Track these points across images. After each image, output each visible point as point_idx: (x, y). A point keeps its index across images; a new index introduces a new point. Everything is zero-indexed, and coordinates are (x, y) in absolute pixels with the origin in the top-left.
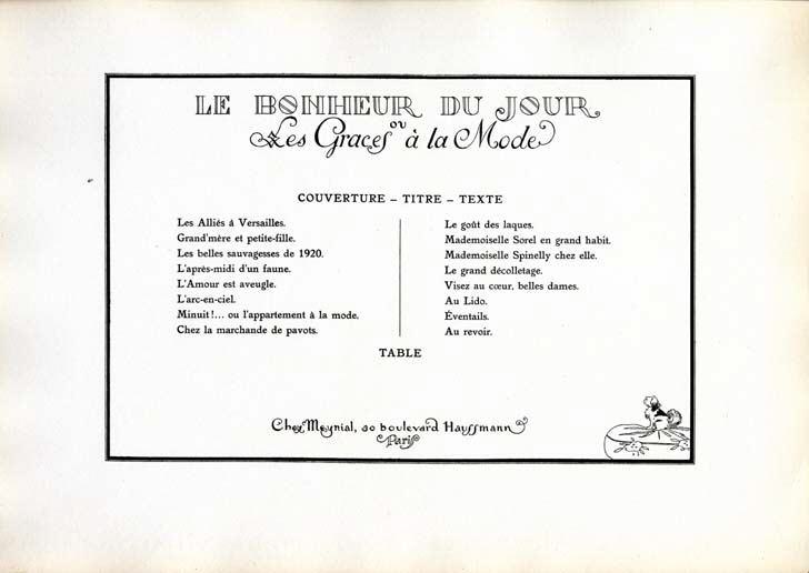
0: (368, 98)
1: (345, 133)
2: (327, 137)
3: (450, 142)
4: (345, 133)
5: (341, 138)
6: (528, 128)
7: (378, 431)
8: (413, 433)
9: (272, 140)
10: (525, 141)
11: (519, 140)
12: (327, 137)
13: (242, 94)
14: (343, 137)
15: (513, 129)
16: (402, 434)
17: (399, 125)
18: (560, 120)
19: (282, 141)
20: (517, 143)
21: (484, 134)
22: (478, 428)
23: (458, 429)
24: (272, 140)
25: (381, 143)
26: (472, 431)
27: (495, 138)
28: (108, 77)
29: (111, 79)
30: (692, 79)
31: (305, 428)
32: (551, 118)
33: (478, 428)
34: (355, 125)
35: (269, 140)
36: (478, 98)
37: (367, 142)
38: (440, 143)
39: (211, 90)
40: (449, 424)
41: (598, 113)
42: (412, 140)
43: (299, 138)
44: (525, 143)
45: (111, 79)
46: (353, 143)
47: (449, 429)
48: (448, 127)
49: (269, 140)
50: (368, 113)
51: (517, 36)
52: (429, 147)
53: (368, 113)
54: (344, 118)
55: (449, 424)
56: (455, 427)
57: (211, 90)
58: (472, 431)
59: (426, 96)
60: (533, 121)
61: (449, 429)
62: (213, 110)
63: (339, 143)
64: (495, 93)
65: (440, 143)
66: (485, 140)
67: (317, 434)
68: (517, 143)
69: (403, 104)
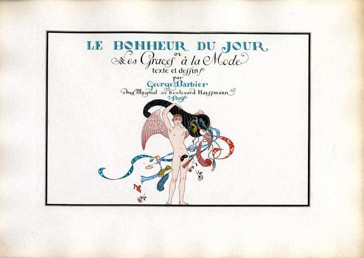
0: (164, 42)
2: (146, 60)
3: (201, 62)
7: (170, 69)
8: (184, 95)
9: (122, 61)
10: (235, 62)
11: (232, 61)
12: (146, 60)
15: (229, 56)
16: (179, 96)
17: (178, 54)
18: (250, 51)
19: (126, 62)
20: (231, 63)
23: (204, 93)
24: (122, 61)
25: (170, 62)
26: (210, 95)
27: (221, 60)
31: (135, 93)
32: (246, 51)
33: (213, 93)
35: (120, 61)
36: (214, 43)
37: (164, 62)
39: (93, 37)
40: (200, 91)
42: (184, 61)
43: (133, 60)
44: (235, 62)
46: (158, 62)
47: (200, 93)
49: (120, 61)
50: (165, 49)
51: (231, 14)
52: (192, 64)
53: (165, 49)
54: (154, 51)
55: (200, 91)
57: (93, 37)
58: (210, 95)
59: (191, 42)
60: (238, 53)
61: (200, 93)
62: (95, 48)
63: (151, 62)
64: (222, 40)
67: (141, 95)
68: (231, 63)
69: (180, 45)
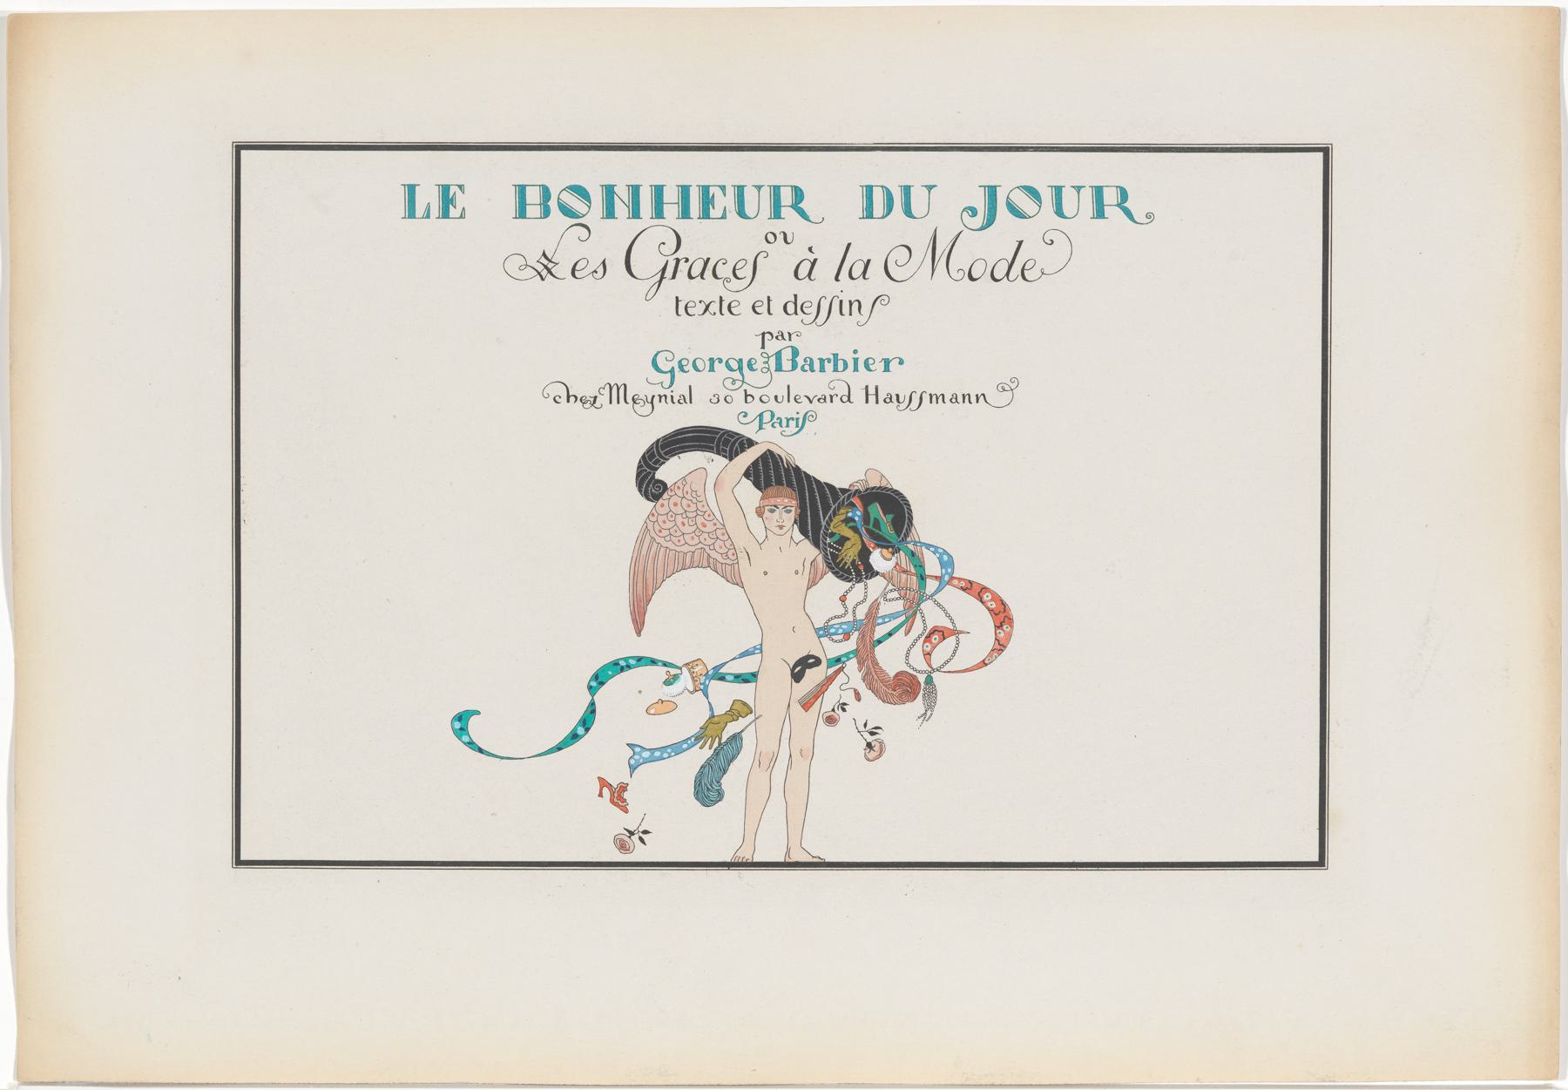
0: (723, 188)
1: (679, 255)
2: (648, 261)
3: (876, 270)
4: (679, 255)
5: (672, 264)
6: (1020, 243)
8: (805, 406)
9: (547, 267)
10: (1015, 268)
11: (1003, 267)
12: (648, 261)
13: (488, 183)
14: (678, 260)
15: (994, 245)
16: (785, 410)
17: (780, 237)
19: (563, 270)
21: (938, 254)
22: (926, 398)
24: (547, 267)
25: (746, 272)
27: (960, 260)
28: (239, 148)
29: (243, 858)
30: (1326, 151)
31: (603, 399)
33: (926, 398)
34: (702, 239)
35: (540, 268)
36: (930, 188)
38: (857, 272)
40: (872, 391)
41: (1149, 216)
43: (595, 263)
45: (243, 858)
46: (696, 271)
47: (872, 399)
48: (874, 239)
49: (540, 268)
50: (724, 217)
53: (724, 217)
54: (682, 226)
55: (872, 391)
56: (882, 396)
59: (832, 185)
60: (1028, 230)
61: (872, 399)
64: (963, 179)
65: (857, 272)
66: (941, 264)
